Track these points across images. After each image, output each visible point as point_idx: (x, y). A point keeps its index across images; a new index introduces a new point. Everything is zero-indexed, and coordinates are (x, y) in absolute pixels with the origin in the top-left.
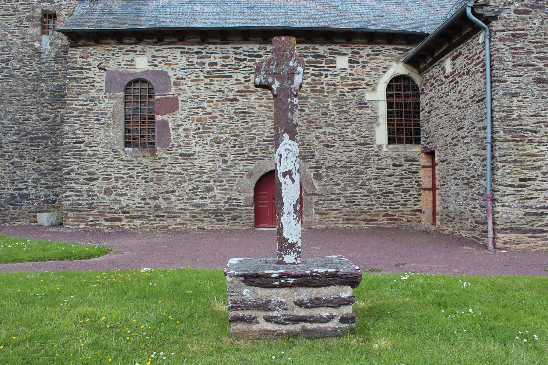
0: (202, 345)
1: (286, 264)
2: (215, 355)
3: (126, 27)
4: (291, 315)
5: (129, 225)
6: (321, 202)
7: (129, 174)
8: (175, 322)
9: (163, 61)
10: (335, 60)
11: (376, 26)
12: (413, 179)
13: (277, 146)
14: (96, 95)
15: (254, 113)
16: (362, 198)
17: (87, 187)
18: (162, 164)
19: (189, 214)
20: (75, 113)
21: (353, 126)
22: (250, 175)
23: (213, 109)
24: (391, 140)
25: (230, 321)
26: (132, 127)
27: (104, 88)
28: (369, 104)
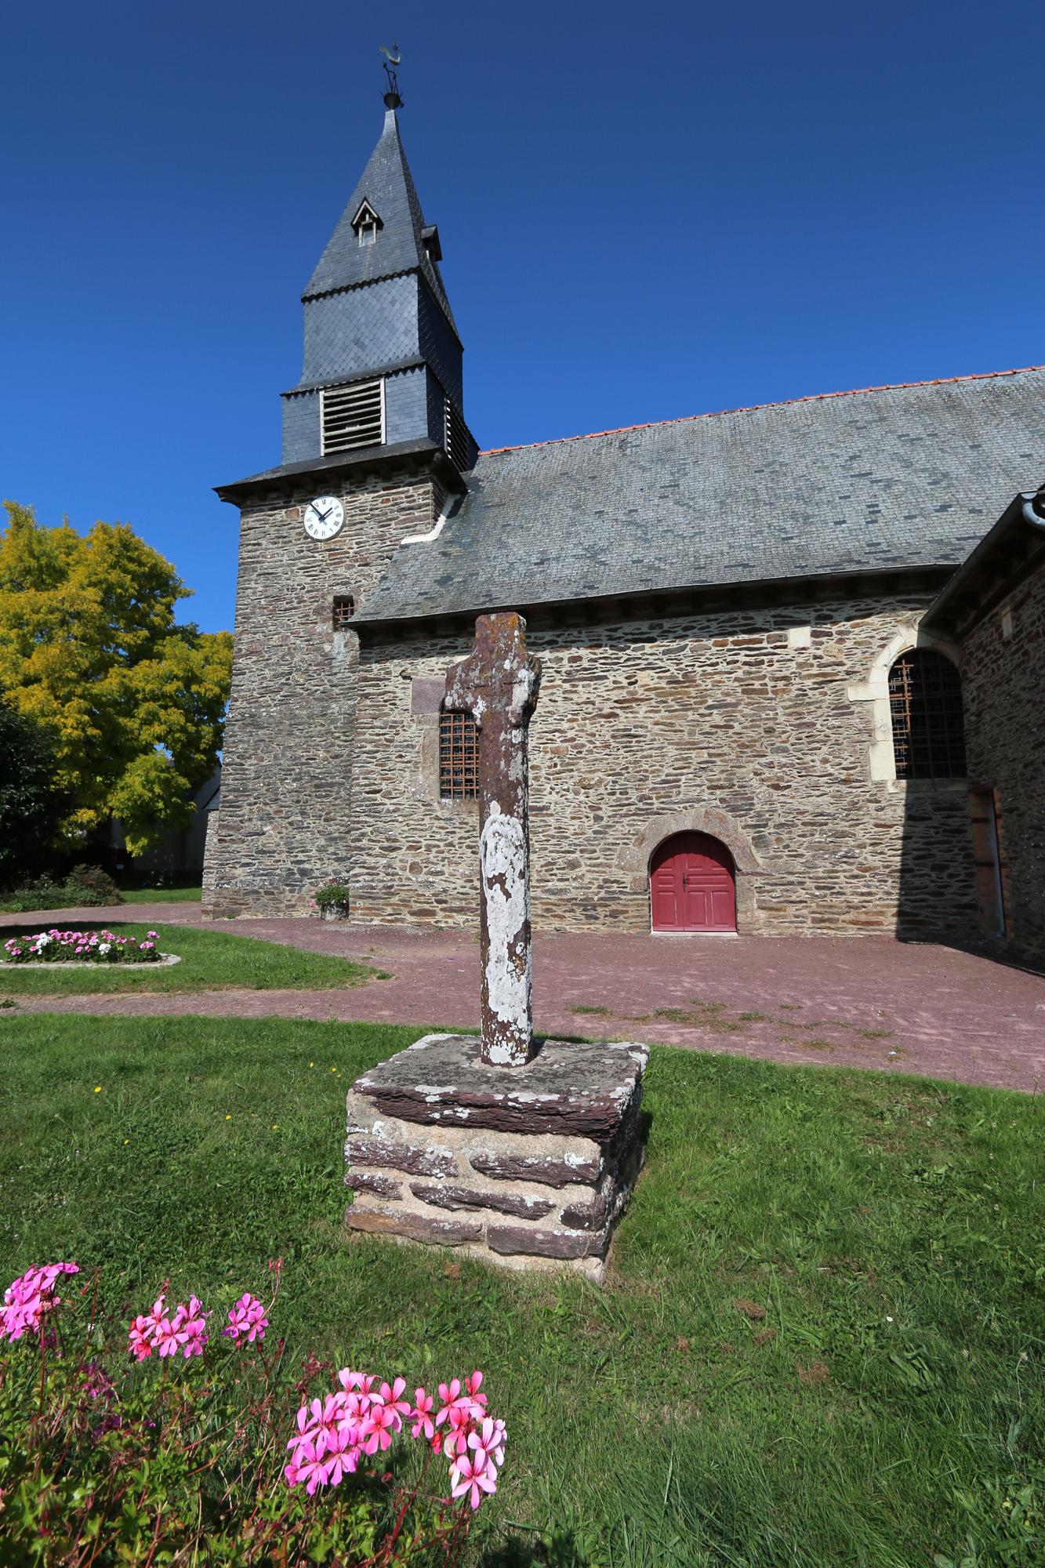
4: (463, 1190)
6: (768, 888)
12: (954, 844)
14: (397, 718)
15: (645, 736)
17: (384, 861)
19: (540, 906)
20: (369, 747)
22: (641, 840)
27: (410, 707)
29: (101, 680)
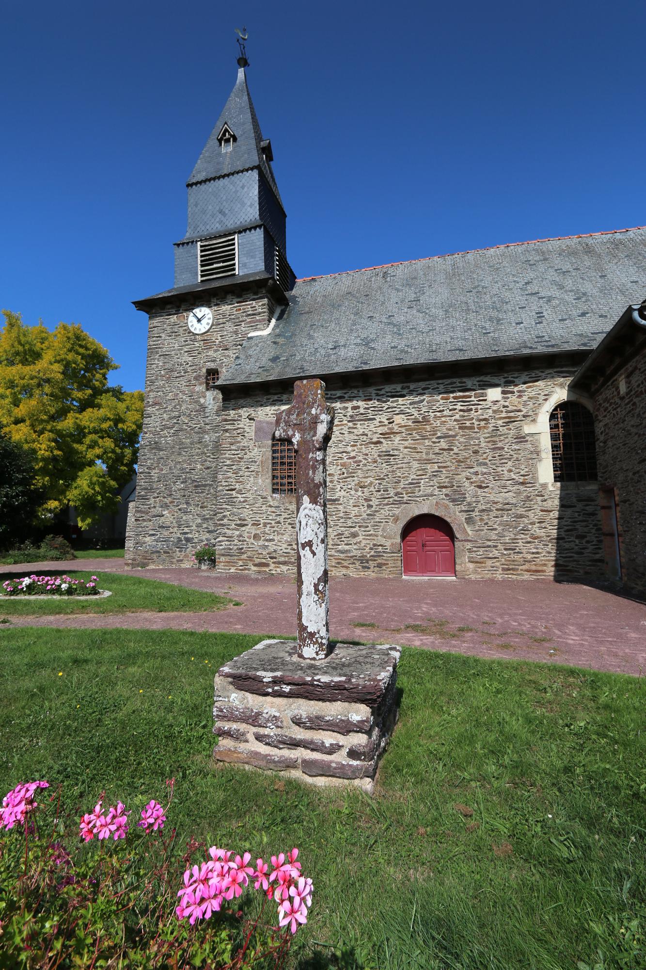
1: (305, 659)
4: (286, 736)
6: (475, 549)
12: (590, 522)
14: (246, 444)
15: (399, 456)
17: (237, 533)
19: (334, 560)
20: (228, 462)
22: (396, 519)
27: (253, 437)
29: (63, 421)
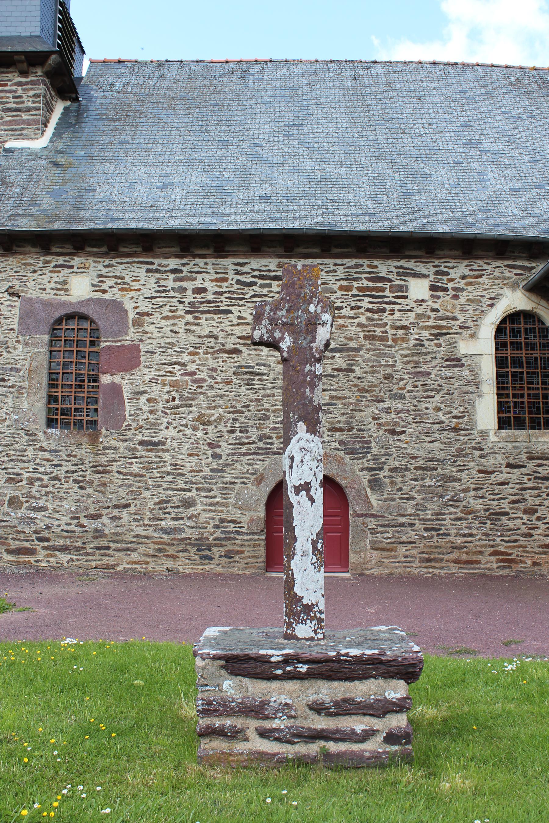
0: (150, 774)
1: (298, 639)
2: (170, 793)
3: (56, 226)
4: (303, 728)
5: (48, 562)
6: (381, 529)
7: (51, 473)
8: (110, 734)
9: (117, 284)
10: (406, 286)
11: (477, 229)
12: (543, 490)
13: (286, 442)
16: (453, 522)
18: (110, 457)
19: (152, 545)
21: (438, 398)
23: (198, 367)
24: (504, 422)
25: (200, 735)
26: (60, 394)
27: (16, 327)
28: (464, 361)
